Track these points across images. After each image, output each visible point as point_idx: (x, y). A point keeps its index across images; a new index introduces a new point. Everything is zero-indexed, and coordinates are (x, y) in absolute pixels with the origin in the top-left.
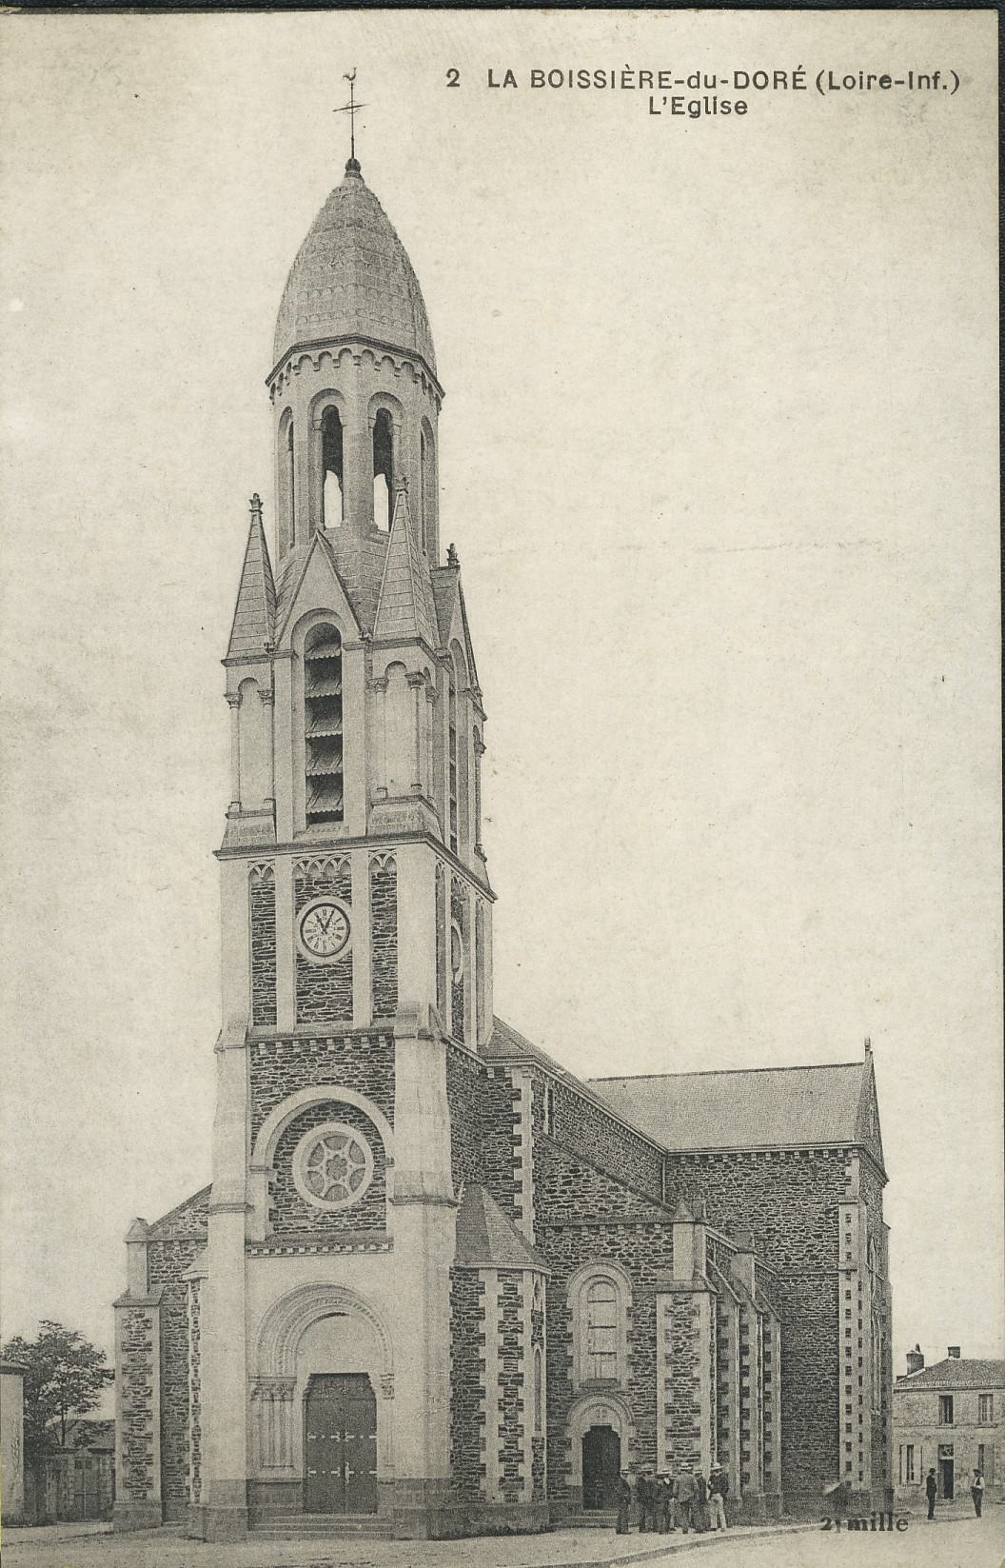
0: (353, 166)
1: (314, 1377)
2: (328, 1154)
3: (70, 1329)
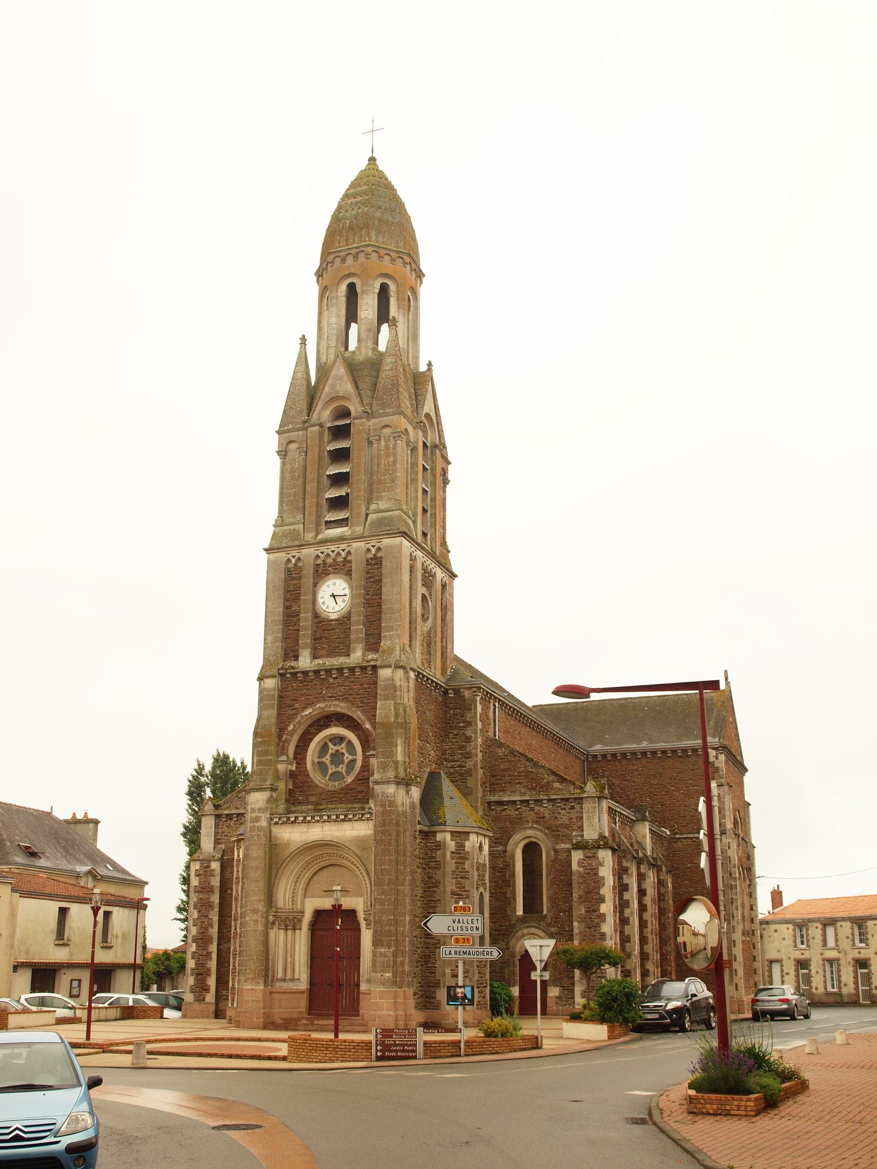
0: (372, 160)
2: (342, 748)
3: (179, 876)
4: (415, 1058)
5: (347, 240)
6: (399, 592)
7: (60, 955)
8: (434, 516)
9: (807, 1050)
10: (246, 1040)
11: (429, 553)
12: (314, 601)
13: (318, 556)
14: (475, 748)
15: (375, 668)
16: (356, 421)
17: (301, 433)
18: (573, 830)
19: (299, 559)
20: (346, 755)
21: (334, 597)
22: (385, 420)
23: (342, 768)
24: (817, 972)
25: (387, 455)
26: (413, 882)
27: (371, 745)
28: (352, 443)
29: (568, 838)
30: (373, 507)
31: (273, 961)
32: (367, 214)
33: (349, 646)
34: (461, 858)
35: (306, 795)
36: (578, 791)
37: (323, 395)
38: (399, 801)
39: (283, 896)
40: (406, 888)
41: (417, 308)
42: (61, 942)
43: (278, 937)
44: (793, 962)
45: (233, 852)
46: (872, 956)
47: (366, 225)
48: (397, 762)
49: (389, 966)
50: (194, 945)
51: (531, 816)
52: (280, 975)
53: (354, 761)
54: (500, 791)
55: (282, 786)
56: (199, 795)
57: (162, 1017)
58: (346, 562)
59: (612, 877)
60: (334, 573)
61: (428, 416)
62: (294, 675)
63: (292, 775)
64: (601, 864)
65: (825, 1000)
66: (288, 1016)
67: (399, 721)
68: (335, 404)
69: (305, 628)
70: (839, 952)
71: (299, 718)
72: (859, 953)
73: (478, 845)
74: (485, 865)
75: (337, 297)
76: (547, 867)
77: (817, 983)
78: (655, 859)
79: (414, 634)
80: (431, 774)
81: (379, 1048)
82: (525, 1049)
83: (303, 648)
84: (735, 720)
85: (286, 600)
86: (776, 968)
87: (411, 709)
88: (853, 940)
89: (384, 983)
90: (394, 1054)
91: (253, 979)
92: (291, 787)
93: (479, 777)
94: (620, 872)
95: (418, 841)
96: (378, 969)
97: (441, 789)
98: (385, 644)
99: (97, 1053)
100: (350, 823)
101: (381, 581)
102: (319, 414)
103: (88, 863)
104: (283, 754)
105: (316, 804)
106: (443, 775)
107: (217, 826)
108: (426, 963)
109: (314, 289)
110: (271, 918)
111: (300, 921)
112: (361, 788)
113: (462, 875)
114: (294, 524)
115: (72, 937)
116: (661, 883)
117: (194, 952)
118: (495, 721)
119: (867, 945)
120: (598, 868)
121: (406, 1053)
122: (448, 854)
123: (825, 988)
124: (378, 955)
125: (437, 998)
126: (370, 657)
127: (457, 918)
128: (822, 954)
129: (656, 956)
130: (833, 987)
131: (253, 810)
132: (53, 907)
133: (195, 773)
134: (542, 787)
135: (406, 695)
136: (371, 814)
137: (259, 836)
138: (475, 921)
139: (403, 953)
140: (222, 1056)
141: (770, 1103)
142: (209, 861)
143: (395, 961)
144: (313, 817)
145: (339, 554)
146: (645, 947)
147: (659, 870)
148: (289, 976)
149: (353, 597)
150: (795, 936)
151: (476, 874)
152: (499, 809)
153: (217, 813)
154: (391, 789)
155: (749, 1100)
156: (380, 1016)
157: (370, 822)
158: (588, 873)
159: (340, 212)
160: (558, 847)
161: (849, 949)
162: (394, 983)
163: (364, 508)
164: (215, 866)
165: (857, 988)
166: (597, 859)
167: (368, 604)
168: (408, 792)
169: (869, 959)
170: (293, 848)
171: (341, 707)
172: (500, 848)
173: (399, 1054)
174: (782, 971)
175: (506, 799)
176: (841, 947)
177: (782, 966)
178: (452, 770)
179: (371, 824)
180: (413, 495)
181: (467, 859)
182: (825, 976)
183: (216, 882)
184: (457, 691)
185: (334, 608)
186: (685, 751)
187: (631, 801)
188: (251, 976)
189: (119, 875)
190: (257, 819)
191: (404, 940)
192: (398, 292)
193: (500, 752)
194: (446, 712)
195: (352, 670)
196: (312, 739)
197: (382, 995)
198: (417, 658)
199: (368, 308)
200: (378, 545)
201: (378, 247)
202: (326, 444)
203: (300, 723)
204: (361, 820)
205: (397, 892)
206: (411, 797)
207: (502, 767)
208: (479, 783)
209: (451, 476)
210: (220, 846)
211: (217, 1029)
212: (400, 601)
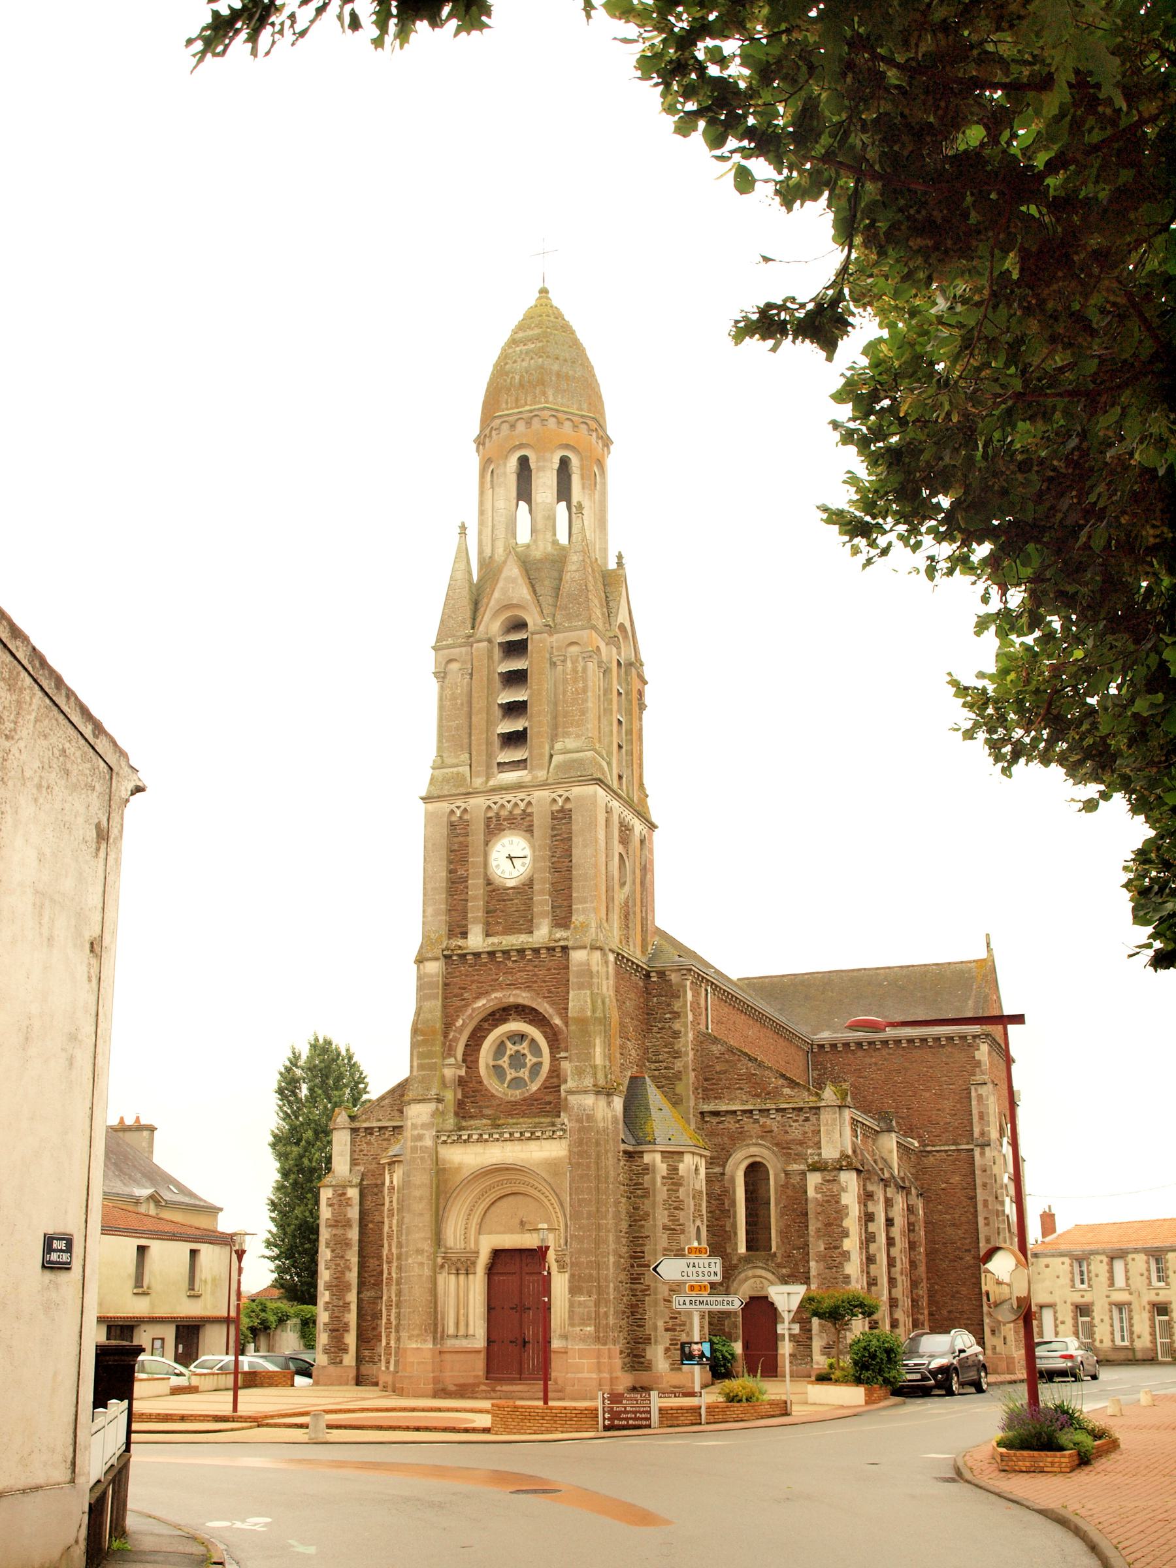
0: (544, 291)
1: (497, 1254)
2: (524, 1047)
4: (649, 1426)
5: (517, 400)
6: (594, 853)
7: (137, 1307)
8: (630, 753)
9: (1110, 1411)
10: (423, 1410)
11: (626, 802)
12: (486, 864)
13: (489, 807)
14: (685, 1045)
15: (565, 949)
16: (536, 637)
17: (463, 649)
18: (808, 1147)
19: (465, 810)
20: (529, 1057)
21: (511, 859)
22: (572, 636)
23: (524, 1073)
24: (1102, 1321)
25: (575, 681)
26: (617, 1214)
27: (562, 1046)
28: (531, 663)
29: (801, 1157)
30: (558, 746)
31: (443, 1314)
32: (542, 367)
33: (531, 921)
34: (673, 1184)
35: (480, 1107)
36: (814, 1099)
37: (492, 602)
38: (599, 1115)
39: (453, 1235)
40: (609, 1221)
41: (604, 484)
42: (140, 1290)
43: (448, 1283)
44: (1069, 1308)
45: (383, 1174)
46: (1172, 1299)
47: (542, 382)
48: (595, 1067)
49: (589, 1319)
50: (327, 1293)
51: (755, 1129)
52: (451, 1330)
53: (540, 1064)
54: (716, 1098)
55: (449, 1096)
56: (294, 1094)
57: (293, 1385)
58: (525, 814)
59: (857, 1206)
60: (510, 828)
61: (622, 627)
62: (463, 957)
63: (461, 1082)
64: (844, 1190)
65: (1113, 1356)
66: (462, 1381)
67: (597, 1015)
68: (508, 614)
69: (475, 898)
70: (1131, 1294)
71: (469, 1011)
72: (1157, 1294)
73: (694, 1168)
74: (701, 1192)
75: (505, 473)
76: (776, 1193)
77: (1103, 1335)
78: (903, 1179)
79: (611, 905)
80: (633, 1079)
81: (607, 1415)
82: (773, 1416)
83: (473, 923)
84: (999, 997)
85: (450, 862)
86: (1047, 1316)
87: (611, 1001)
88: (1149, 1278)
89: (583, 1340)
90: (624, 1423)
91: (418, 1335)
92: (460, 1096)
93: (691, 1081)
94: (867, 1196)
95: (622, 1163)
96: (576, 1322)
97: (647, 1099)
98: (577, 919)
99: (251, 1427)
100: (538, 1142)
101: (570, 839)
102: (487, 627)
103: (148, 1184)
104: (450, 1056)
105: (494, 1118)
106: (648, 1080)
107: (353, 1142)
108: (633, 1313)
109: (473, 461)
110: (440, 1261)
111: (474, 1263)
112: (549, 1098)
113: (676, 1205)
114: (457, 766)
115: (153, 1285)
116: (910, 1209)
117: (327, 1303)
118: (707, 1009)
119: (1168, 1284)
120: (839, 1194)
121: (637, 1423)
122: (659, 1180)
123: (1113, 1341)
124: (576, 1305)
125: (648, 1357)
126: (558, 936)
127: (692, 1261)
128: (1108, 1297)
129: (905, 1303)
130: (1123, 1340)
131: (414, 1126)
132: (133, 1243)
133: (288, 1064)
134: (769, 1093)
135: (604, 982)
136: (564, 1131)
137: (422, 1158)
138: (713, 1265)
139: (607, 1301)
140: (407, 1429)
141: (1084, 1460)
142: (344, 1187)
143: (597, 1313)
144: (491, 1135)
145: (516, 804)
146: (893, 1291)
147: (908, 1193)
148: (462, 1332)
149: (535, 860)
150: (1072, 1273)
151: (692, 1203)
152: (715, 1120)
153: (353, 1126)
154: (589, 1100)
155: (1064, 1456)
156: (580, 1380)
157: (563, 1141)
158: (828, 1201)
159: (506, 364)
160: (789, 1168)
161: (1144, 1290)
162: (598, 1339)
163: (547, 747)
164: (353, 1193)
165: (1154, 1341)
166: (839, 1182)
167: (555, 869)
168: (609, 1104)
169: (1171, 1303)
170: (466, 1173)
171: (523, 997)
172: (717, 1170)
173: (631, 1422)
174: (1056, 1319)
175: (724, 1108)
176: (1133, 1287)
177: (1055, 1312)
178: (656, 1073)
179: (564, 1144)
180: (607, 729)
181: (681, 1185)
182: (1112, 1326)
183: (354, 1213)
184: (662, 974)
185: (511, 873)
186: (937, 1039)
187: (879, 1113)
188: (416, 1332)
189: (186, 1200)
190: (420, 1138)
191: (607, 1287)
192: (582, 468)
193: (716, 1049)
194: (647, 1000)
195: (536, 951)
196: (485, 1037)
197: (582, 1354)
198: (614, 936)
199: (545, 484)
200: (566, 794)
201: (557, 410)
202: (496, 664)
203: (471, 1017)
204: (551, 1138)
205: (599, 1227)
206: (613, 1110)
207: (718, 1068)
208: (691, 1089)
209: (647, 699)
210: (358, 1168)
211: (370, 1397)
212: (596, 865)
